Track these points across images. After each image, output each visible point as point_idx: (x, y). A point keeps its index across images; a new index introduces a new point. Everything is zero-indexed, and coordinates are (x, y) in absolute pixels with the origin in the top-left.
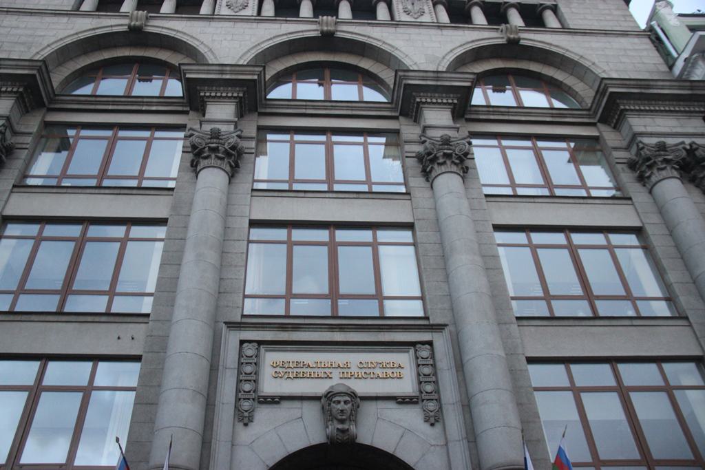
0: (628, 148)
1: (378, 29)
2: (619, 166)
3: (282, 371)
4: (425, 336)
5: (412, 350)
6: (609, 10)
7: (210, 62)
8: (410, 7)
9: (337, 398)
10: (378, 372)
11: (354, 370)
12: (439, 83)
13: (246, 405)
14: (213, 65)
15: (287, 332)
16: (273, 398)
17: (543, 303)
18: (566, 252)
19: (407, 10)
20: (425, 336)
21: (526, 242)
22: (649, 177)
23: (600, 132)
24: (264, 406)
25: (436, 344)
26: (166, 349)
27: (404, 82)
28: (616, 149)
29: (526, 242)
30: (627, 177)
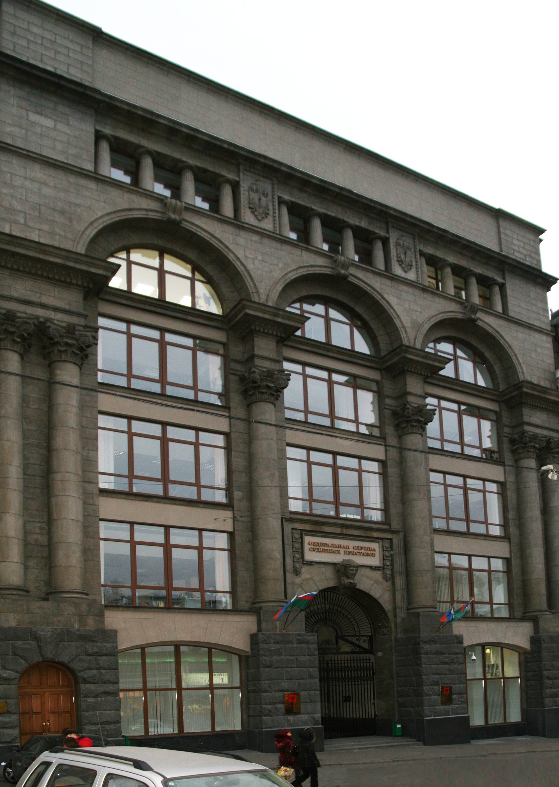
0: (513, 427)
1: (370, 276)
2: (504, 438)
3: (316, 548)
4: (389, 536)
5: (381, 543)
6: (519, 246)
7: (253, 300)
8: (403, 257)
9: (351, 568)
10: (363, 551)
11: (351, 550)
12: (426, 361)
13: (298, 565)
14: (255, 302)
15: (315, 524)
16: (311, 562)
17: (363, 468)
18: (325, 384)
19: (400, 260)
20: (389, 536)
21: (301, 371)
22: (520, 453)
23: (501, 409)
24: (305, 566)
25: (395, 541)
26: (24, 445)
27: (404, 355)
28: (506, 426)
29: (301, 371)
30: (506, 446)
